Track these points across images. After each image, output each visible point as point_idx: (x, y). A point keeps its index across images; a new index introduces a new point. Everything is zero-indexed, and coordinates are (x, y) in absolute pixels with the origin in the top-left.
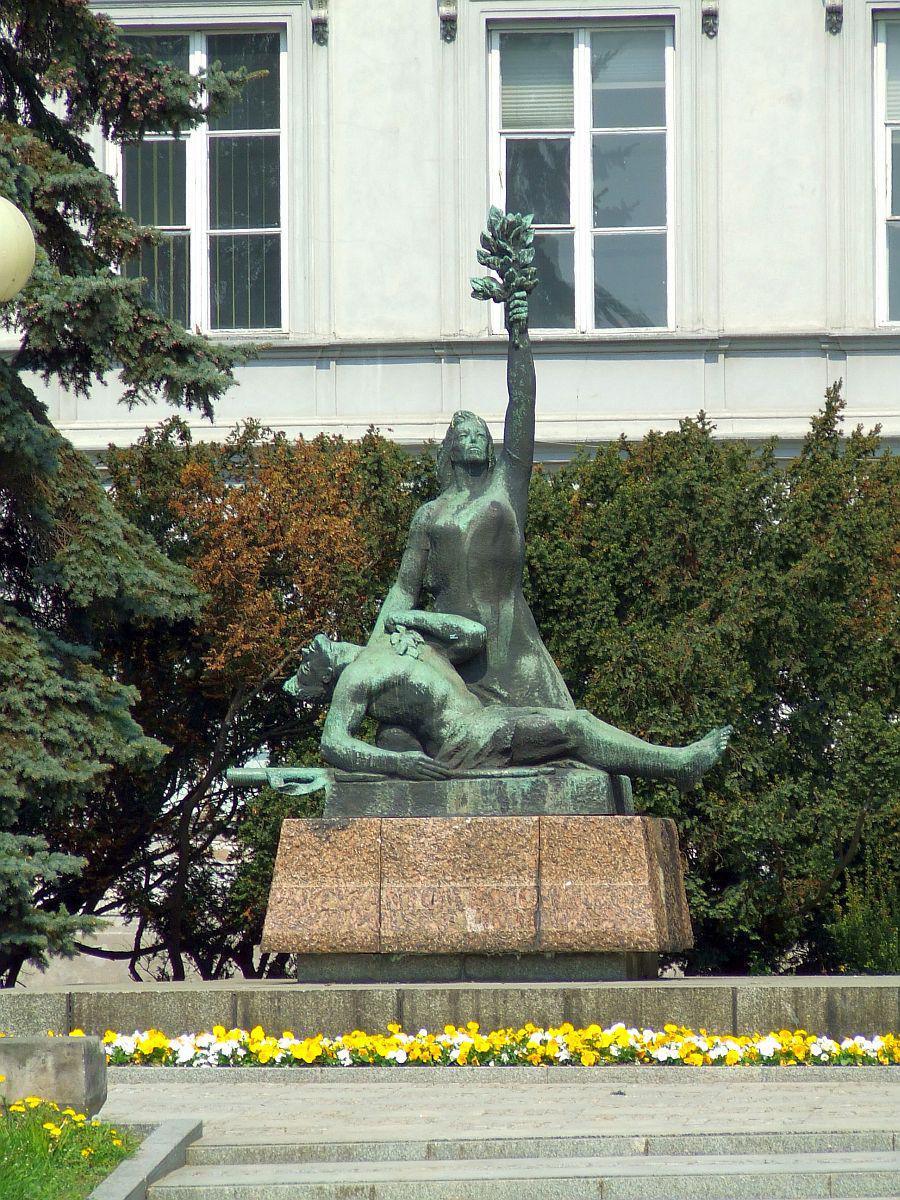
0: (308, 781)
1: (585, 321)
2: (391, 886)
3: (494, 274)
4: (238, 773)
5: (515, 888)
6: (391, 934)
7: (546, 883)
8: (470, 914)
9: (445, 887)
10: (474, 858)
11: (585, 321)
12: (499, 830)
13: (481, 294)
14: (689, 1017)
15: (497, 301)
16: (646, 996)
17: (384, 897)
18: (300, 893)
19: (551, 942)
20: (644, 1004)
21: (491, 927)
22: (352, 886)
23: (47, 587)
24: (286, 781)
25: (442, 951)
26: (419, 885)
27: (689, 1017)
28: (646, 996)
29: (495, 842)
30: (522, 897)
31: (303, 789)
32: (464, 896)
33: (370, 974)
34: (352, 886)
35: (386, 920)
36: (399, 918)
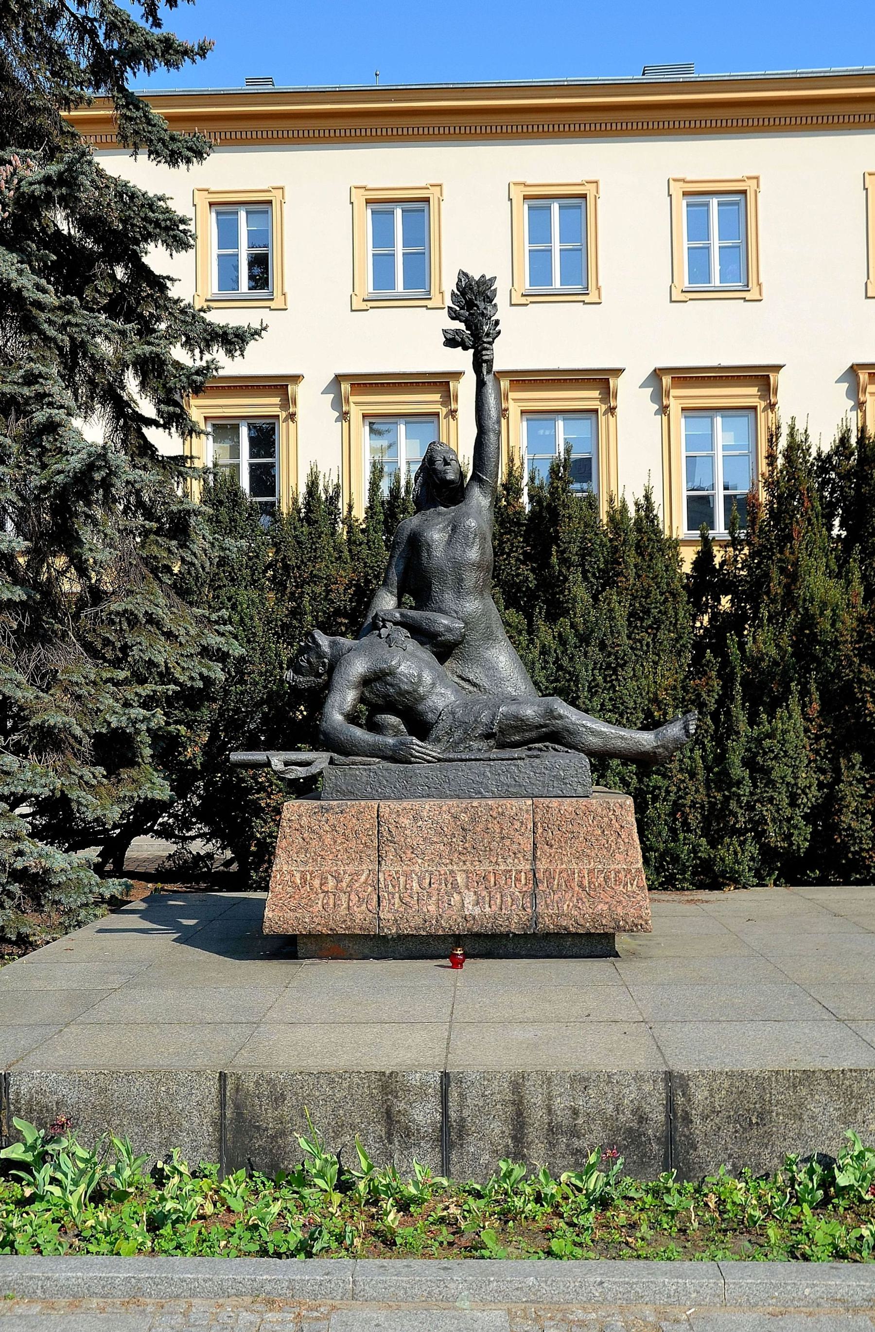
0: (307, 764)
1: (716, 281)
2: (390, 867)
3: (462, 326)
4: (250, 757)
5: (511, 871)
6: (390, 916)
7: (542, 866)
8: (470, 898)
9: (443, 869)
10: (467, 840)
11: (716, 281)
12: (495, 814)
13: (452, 342)
14: (835, 1109)
15: (465, 348)
16: (777, 1080)
17: (382, 880)
18: (298, 875)
19: (547, 924)
20: (774, 1092)
21: (488, 909)
22: (350, 869)
23: (81, 84)
24: (286, 765)
25: (440, 932)
26: (417, 868)
27: (835, 1109)
28: (777, 1080)
29: (490, 826)
30: (518, 880)
31: (300, 772)
32: (460, 879)
33: (366, 951)
34: (350, 869)
35: (384, 903)
36: (397, 900)
